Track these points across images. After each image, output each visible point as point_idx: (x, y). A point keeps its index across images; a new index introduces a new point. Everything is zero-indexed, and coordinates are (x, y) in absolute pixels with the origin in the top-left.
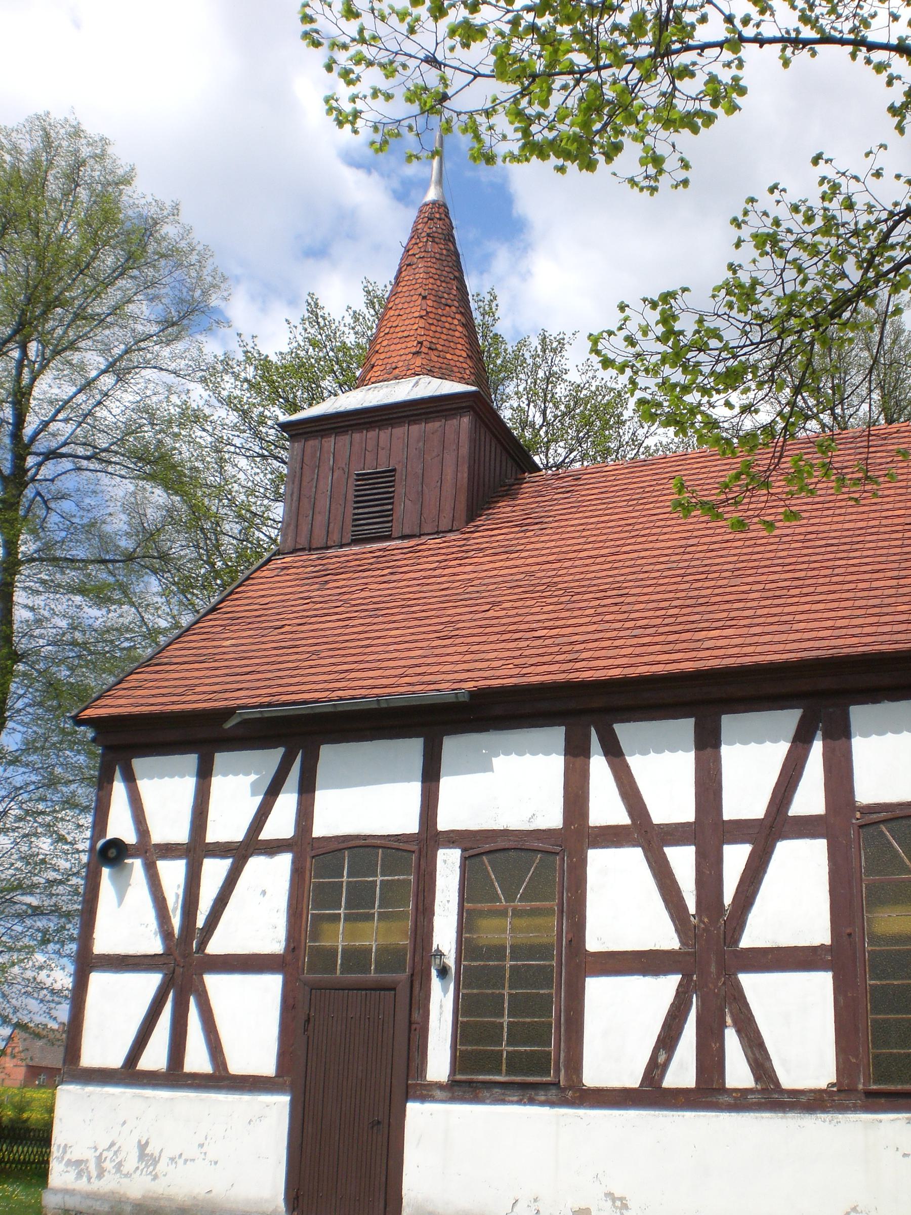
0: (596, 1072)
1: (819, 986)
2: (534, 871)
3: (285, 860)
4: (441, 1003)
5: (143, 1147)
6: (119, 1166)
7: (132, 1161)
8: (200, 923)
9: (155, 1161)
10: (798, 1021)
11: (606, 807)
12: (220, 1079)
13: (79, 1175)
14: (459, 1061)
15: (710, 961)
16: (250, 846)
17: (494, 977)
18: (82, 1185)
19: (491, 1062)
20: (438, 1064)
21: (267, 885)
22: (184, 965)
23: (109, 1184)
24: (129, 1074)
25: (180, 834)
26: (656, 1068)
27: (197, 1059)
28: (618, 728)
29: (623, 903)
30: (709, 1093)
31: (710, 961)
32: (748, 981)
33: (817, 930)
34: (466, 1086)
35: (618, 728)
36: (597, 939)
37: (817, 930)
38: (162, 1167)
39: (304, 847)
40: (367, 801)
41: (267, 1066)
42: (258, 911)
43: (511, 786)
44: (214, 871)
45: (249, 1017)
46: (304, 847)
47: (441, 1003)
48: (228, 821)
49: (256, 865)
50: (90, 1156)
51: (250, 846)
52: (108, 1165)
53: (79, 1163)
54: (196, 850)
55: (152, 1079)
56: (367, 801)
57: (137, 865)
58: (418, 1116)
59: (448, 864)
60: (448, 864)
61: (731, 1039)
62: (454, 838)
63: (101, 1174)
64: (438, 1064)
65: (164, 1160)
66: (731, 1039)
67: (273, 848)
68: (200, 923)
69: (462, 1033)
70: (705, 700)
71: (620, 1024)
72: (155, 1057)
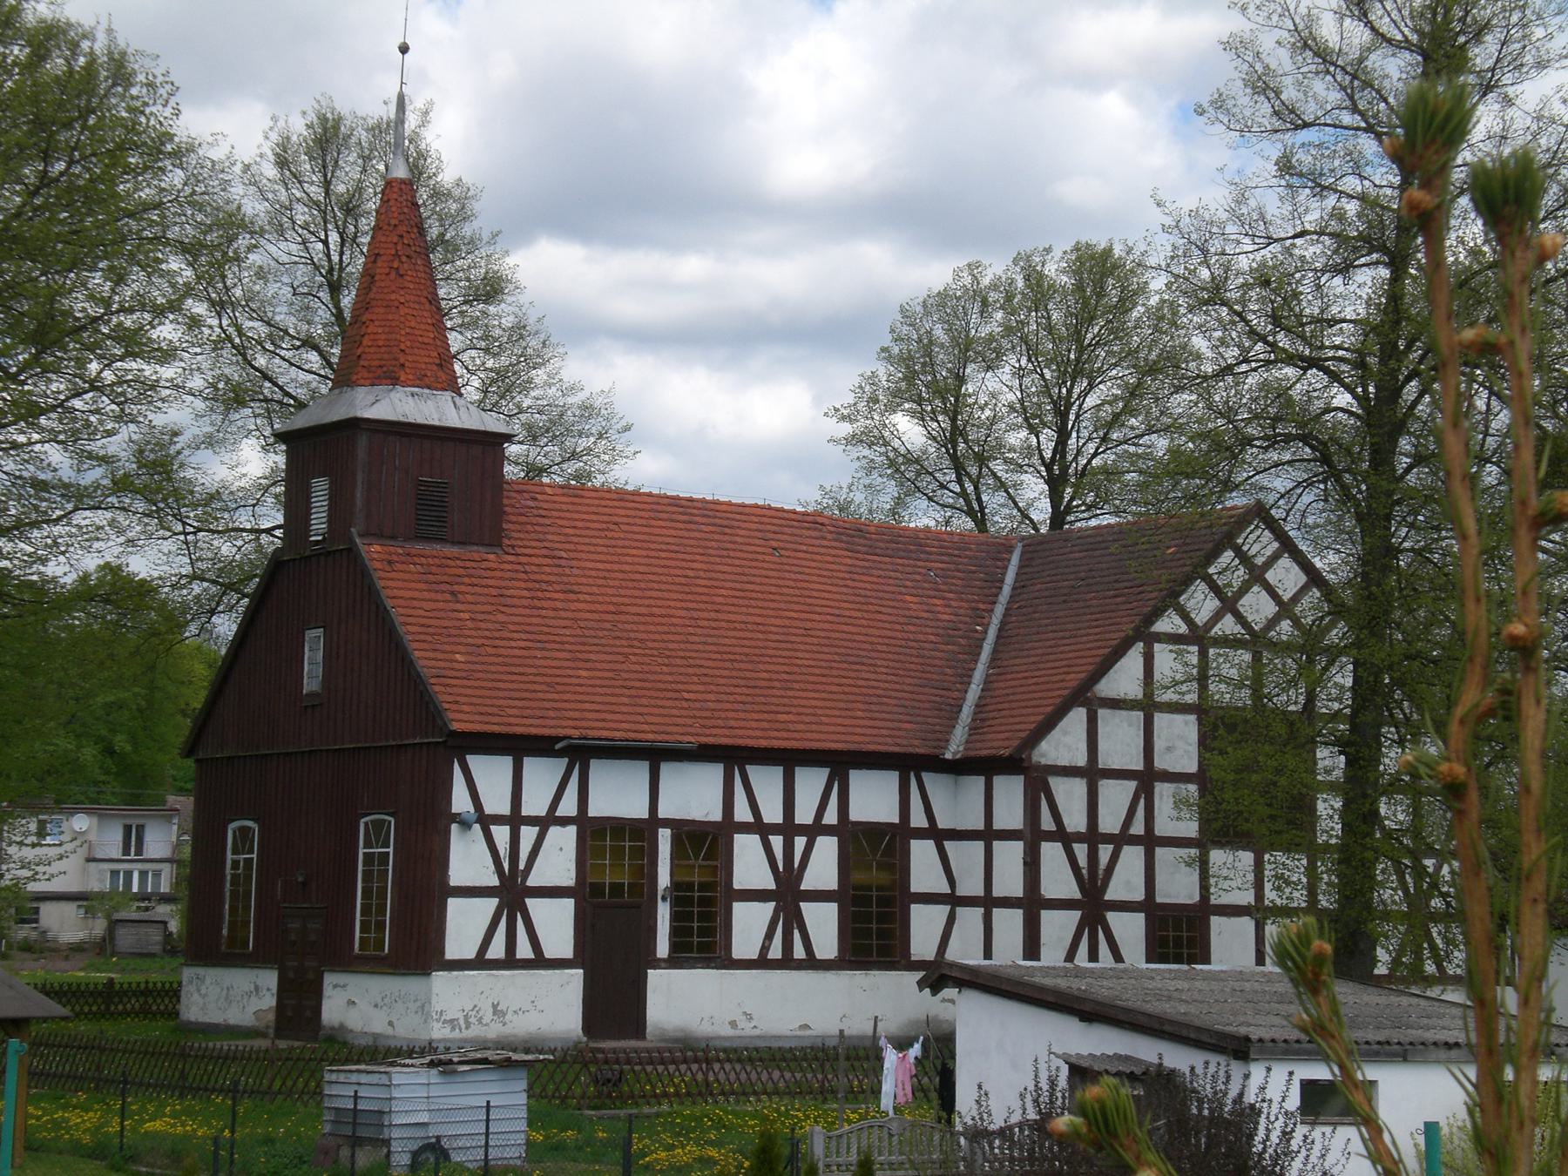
0: (738, 953)
1: (831, 909)
2: (705, 844)
3: (572, 830)
4: (664, 912)
5: (495, 1006)
6: (480, 1020)
7: (488, 1015)
8: (522, 867)
9: (504, 1014)
10: (823, 923)
11: (742, 813)
12: (540, 962)
13: (453, 1029)
14: (675, 947)
15: (788, 895)
16: (549, 820)
17: (688, 901)
18: (456, 1034)
19: (688, 947)
20: (663, 949)
21: (826, 853)
22: (512, 893)
23: (475, 1032)
24: (480, 962)
25: (505, 810)
26: (765, 949)
27: (524, 950)
28: (748, 767)
29: (750, 864)
30: (787, 962)
31: (788, 895)
32: (1077, 895)
33: (568, 878)
34: (674, 962)
35: (748, 767)
36: (916, 887)
37: (568, 878)
38: (508, 1017)
39: (582, 820)
40: (618, 793)
41: (568, 953)
42: (557, 861)
43: (693, 794)
44: (528, 834)
45: (555, 923)
46: (582, 820)
47: (664, 912)
48: (535, 804)
49: (554, 832)
50: (460, 1015)
51: (549, 820)
52: (472, 1020)
53: (452, 1021)
54: (515, 820)
55: (495, 965)
56: (618, 793)
57: (477, 827)
58: (654, 976)
59: (665, 837)
60: (665, 837)
61: (796, 934)
62: (667, 823)
63: (468, 1026)
64: (663, 949)
65: (510, 1013)
66: (796, 934)
67: (564, 821)
68: (522, 867)
69: (675, 932)
70: (789, 760)
71: (749, 925)
72: (497, 950)
